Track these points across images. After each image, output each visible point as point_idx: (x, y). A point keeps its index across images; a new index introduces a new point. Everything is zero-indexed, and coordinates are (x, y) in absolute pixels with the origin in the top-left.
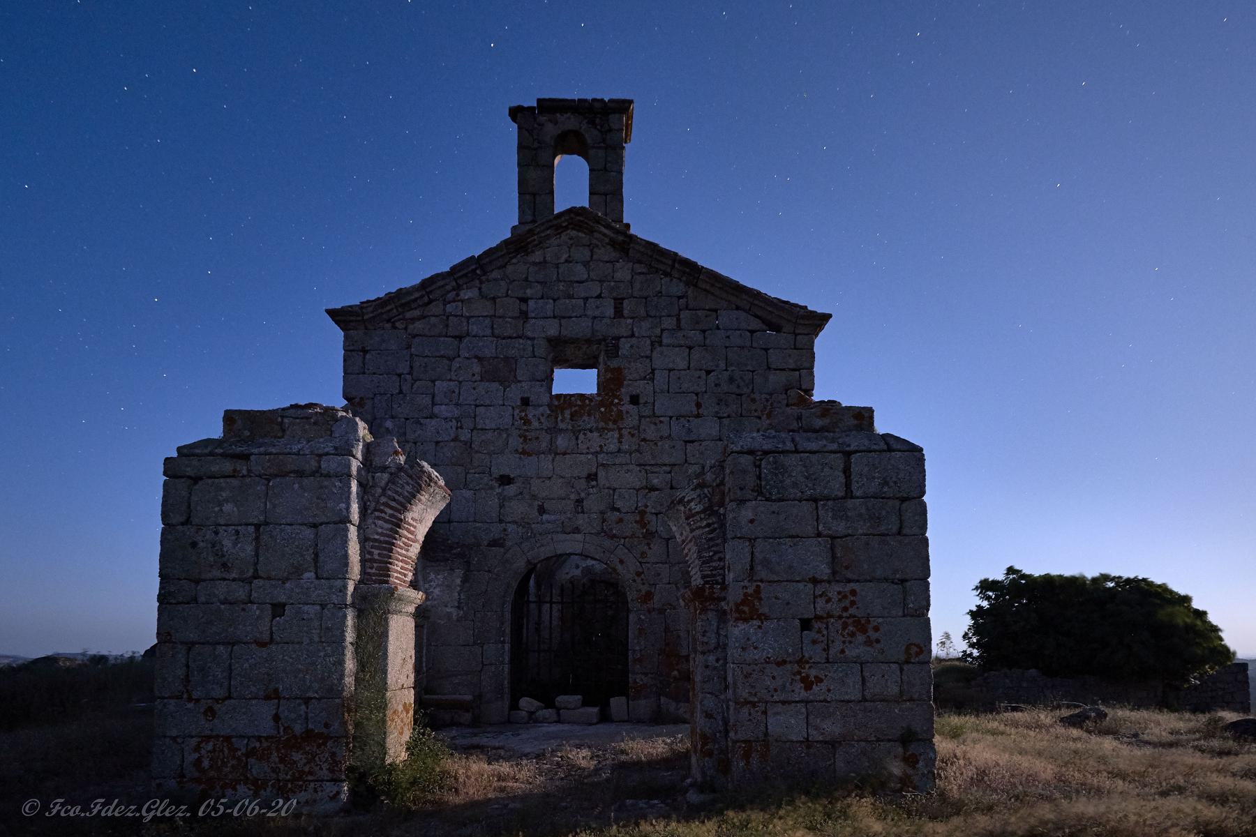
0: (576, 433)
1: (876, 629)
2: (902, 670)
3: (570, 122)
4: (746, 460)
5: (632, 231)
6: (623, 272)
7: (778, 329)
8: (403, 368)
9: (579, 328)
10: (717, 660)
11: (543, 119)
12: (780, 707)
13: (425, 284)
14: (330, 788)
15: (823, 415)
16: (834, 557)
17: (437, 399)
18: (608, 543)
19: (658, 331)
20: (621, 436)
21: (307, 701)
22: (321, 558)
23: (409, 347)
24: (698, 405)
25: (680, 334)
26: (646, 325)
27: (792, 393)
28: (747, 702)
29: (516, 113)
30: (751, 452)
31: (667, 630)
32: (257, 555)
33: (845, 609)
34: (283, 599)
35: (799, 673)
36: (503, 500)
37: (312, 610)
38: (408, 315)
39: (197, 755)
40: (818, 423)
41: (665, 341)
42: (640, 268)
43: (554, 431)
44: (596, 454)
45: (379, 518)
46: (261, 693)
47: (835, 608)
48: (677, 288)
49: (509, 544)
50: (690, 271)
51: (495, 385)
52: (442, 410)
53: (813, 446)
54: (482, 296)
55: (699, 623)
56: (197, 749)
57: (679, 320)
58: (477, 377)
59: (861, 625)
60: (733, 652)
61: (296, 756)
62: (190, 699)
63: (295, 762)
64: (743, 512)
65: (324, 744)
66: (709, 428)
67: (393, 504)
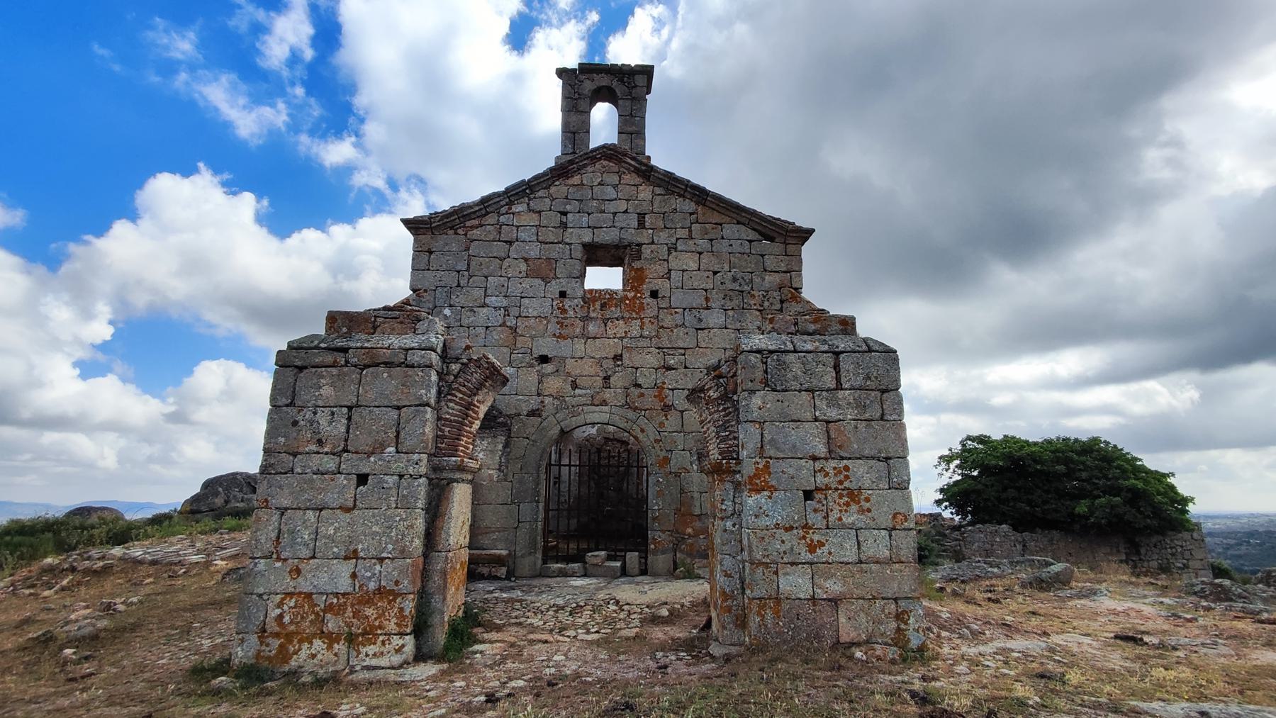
0: (605, 321)
1: (867, 500)
2: (890, 536)
3: (604, 80)
4: (754, 358)
5: (653, 162)
6: (645, 192)
7: (772, 240)
8: (462, 266)
9: (607, 236)
10: (734, 525)
11: (582, 77)
12: (789, 569)
13: (484, 200)
14: (397, 641)
15: (815, 321)
16: (829, 437)
17: (489, 292)
18: (631, 414)
19: (673, 240)
20: (643, 323)
21: (381, 560)
22: (402, 434)
23: (467, 249)
24: (707, 299)
25: (691, 242)
26: (664, 235)
27: (785, 290)
28: (761, 563)
29: (561, 73)
30: (759, 352)
31: (682, 491)
32: (348, 432)
33: (841, 482)
34: (365, 470)
35: (804, 538)
36: (542, 378)
37: (391, 480)
38: (468, 224)
39: (278, 611)
40: (812, 327)
41: (679, 248)
42: (658, 191)
43: (586, 319)
44: (621, 338)
45: (450, 401)
46: (343, 553)
47: (832, 481)
48: (689, 206)
49: (544, 415)
50: (700, 195)
51: (538, 282)
52: (491, 300)
53: (809, 347)
54: (530, 210)
55: (718, 492)
56: (280, 605)
57: (690, 231)
58: (524, 274)
59: (853, 496)
60: (748, 519)
61: (369, 611)
62: (278, 559)
63: (367, 617)
64: (754, 400)
65: (394, 600)
66: (715, 318)
67: (464, 389)
